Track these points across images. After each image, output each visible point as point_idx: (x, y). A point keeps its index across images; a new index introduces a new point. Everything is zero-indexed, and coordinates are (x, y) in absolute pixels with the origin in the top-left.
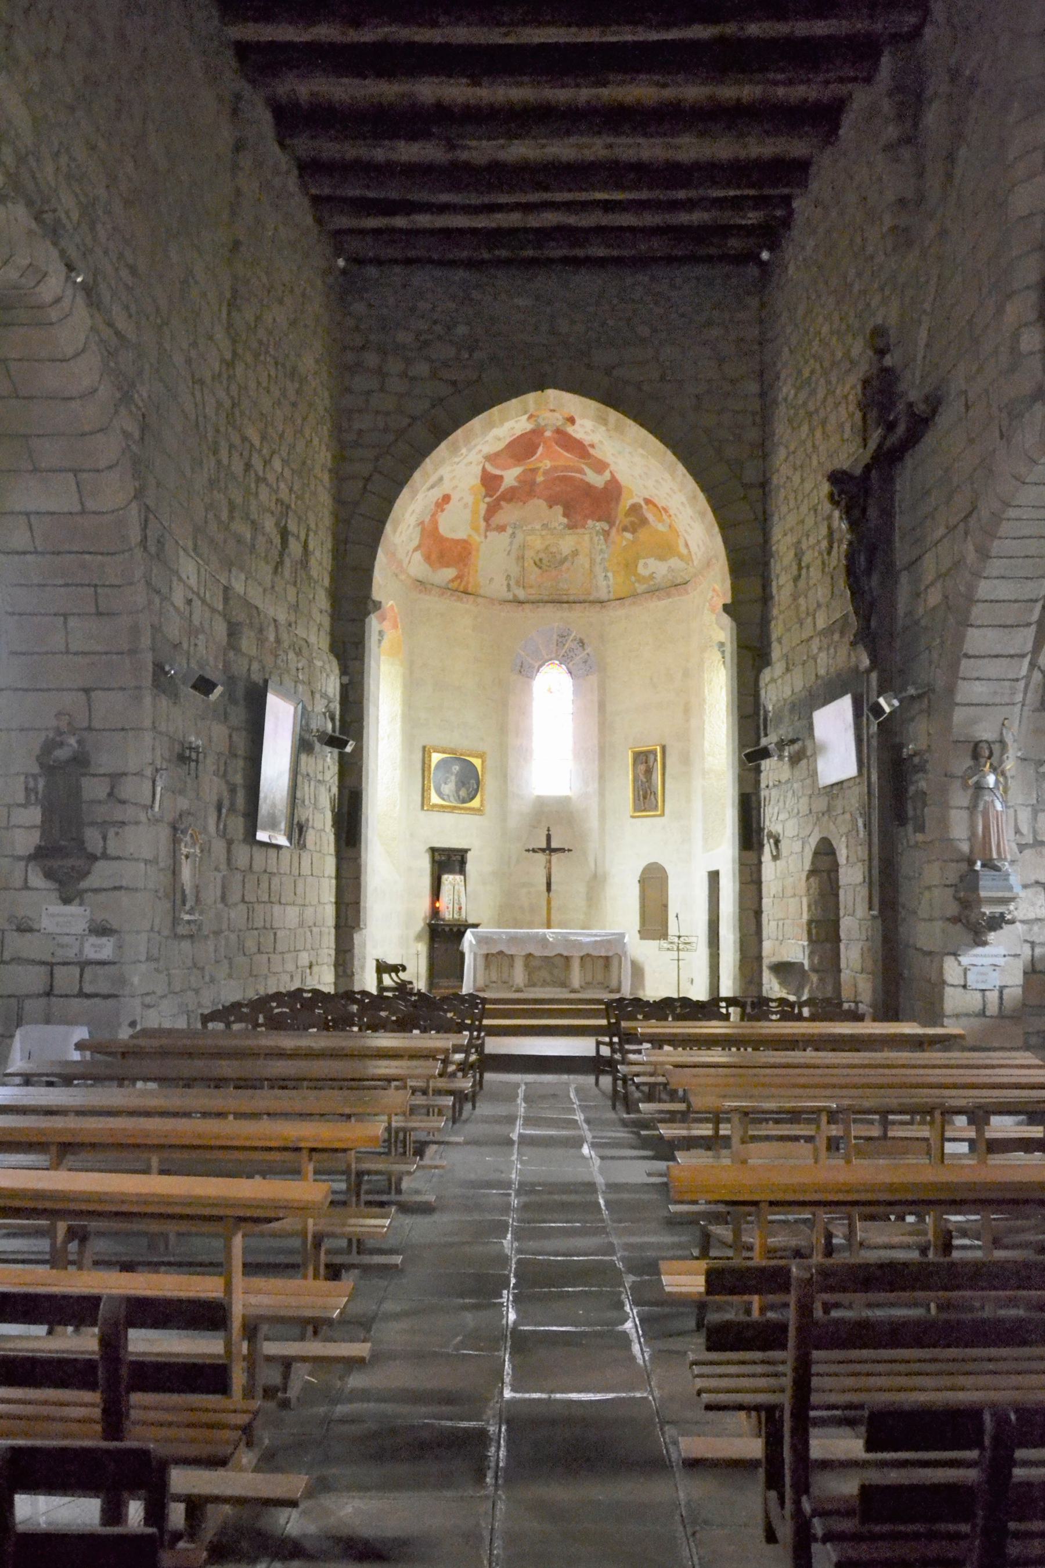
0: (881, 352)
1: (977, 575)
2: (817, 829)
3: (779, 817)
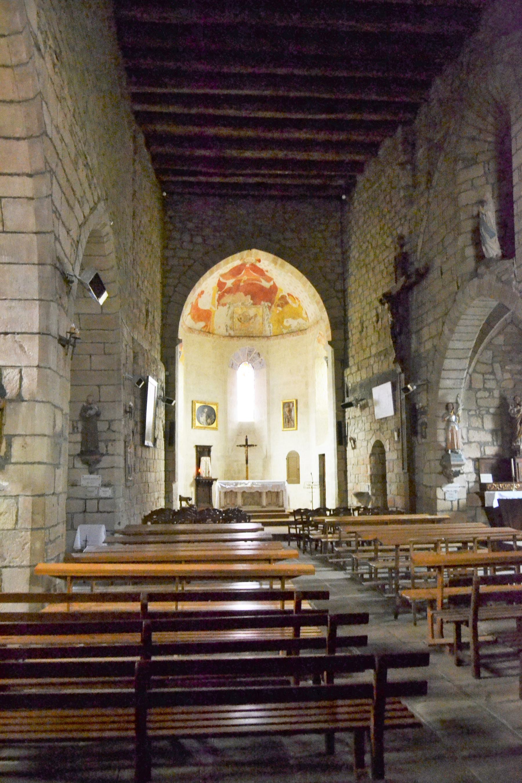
0: (402, 246)
1: (449, 339)
2: (374, 437)
3: (353, 431)
